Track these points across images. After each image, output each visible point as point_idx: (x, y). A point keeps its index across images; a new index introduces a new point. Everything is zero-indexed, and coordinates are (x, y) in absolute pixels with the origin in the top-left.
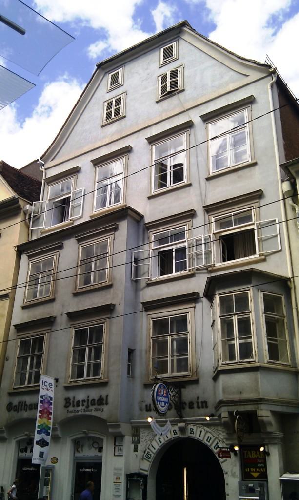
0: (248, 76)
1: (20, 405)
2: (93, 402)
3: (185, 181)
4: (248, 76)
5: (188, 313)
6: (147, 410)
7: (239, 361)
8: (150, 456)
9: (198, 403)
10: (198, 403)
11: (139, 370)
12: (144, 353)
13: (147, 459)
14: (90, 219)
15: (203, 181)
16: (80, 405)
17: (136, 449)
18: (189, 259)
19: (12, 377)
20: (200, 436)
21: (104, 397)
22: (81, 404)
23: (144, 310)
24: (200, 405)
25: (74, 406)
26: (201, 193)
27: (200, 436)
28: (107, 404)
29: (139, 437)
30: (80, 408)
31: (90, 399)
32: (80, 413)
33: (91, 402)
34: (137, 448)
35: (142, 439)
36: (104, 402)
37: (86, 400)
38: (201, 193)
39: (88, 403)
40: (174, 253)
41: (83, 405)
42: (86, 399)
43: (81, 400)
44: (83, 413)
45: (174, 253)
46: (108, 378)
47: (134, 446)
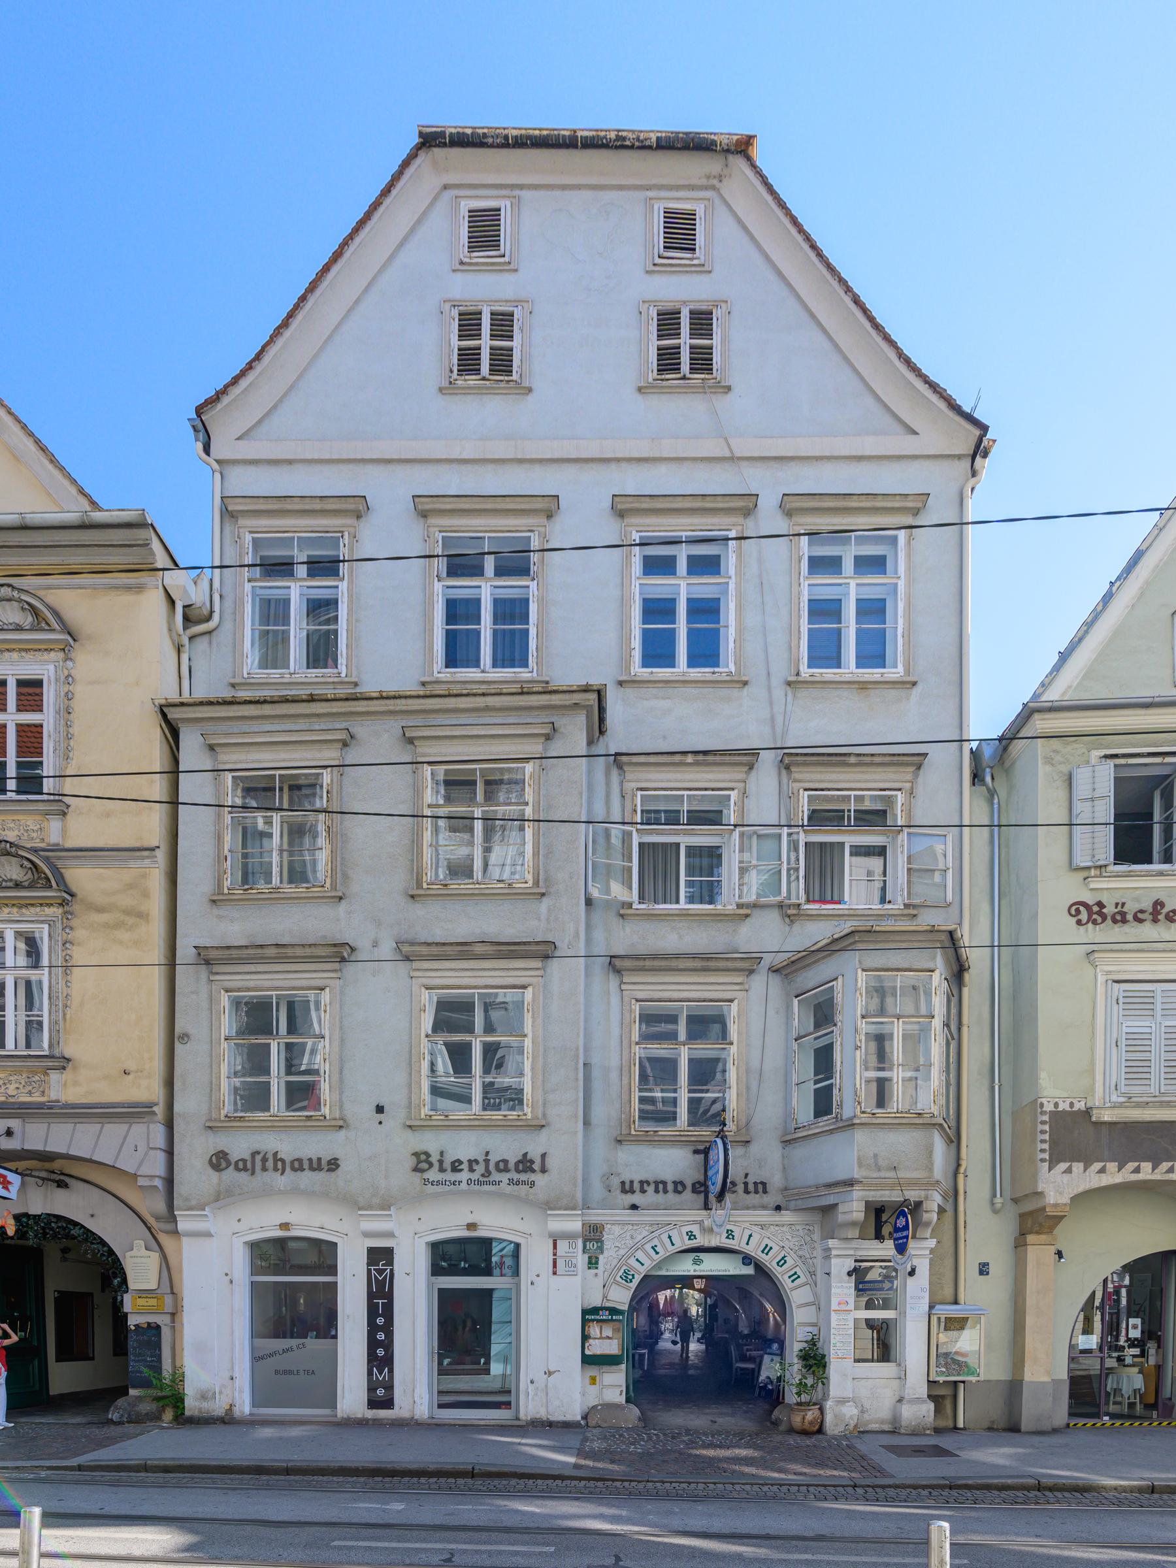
0: (915, 433)
1: (258, 1158)
3: (728, 666)
4: (915, 433)
5: (731, 1001)
6: (624, 1191)
8: (630, 1277)
9: (746, 1184)
10: (746, 1184)
11: (600, 1112)
12: (614, 1075)
17: (593, 1263)
19: (213, 1087)
20: (747, 1244)
21: (535, 1155)
23: (534, 557)
24: (751, 1187)
25: (442, 1170)
26: (773, 719)
28: (544, 1170)
29: (602, 1242)
31: (494, 1159)
34: (597, 1263)
36: (536, 1166)
38: (773, 719)
41: (472, 1170)
42: (481, 1159)
47: (590, 1258)
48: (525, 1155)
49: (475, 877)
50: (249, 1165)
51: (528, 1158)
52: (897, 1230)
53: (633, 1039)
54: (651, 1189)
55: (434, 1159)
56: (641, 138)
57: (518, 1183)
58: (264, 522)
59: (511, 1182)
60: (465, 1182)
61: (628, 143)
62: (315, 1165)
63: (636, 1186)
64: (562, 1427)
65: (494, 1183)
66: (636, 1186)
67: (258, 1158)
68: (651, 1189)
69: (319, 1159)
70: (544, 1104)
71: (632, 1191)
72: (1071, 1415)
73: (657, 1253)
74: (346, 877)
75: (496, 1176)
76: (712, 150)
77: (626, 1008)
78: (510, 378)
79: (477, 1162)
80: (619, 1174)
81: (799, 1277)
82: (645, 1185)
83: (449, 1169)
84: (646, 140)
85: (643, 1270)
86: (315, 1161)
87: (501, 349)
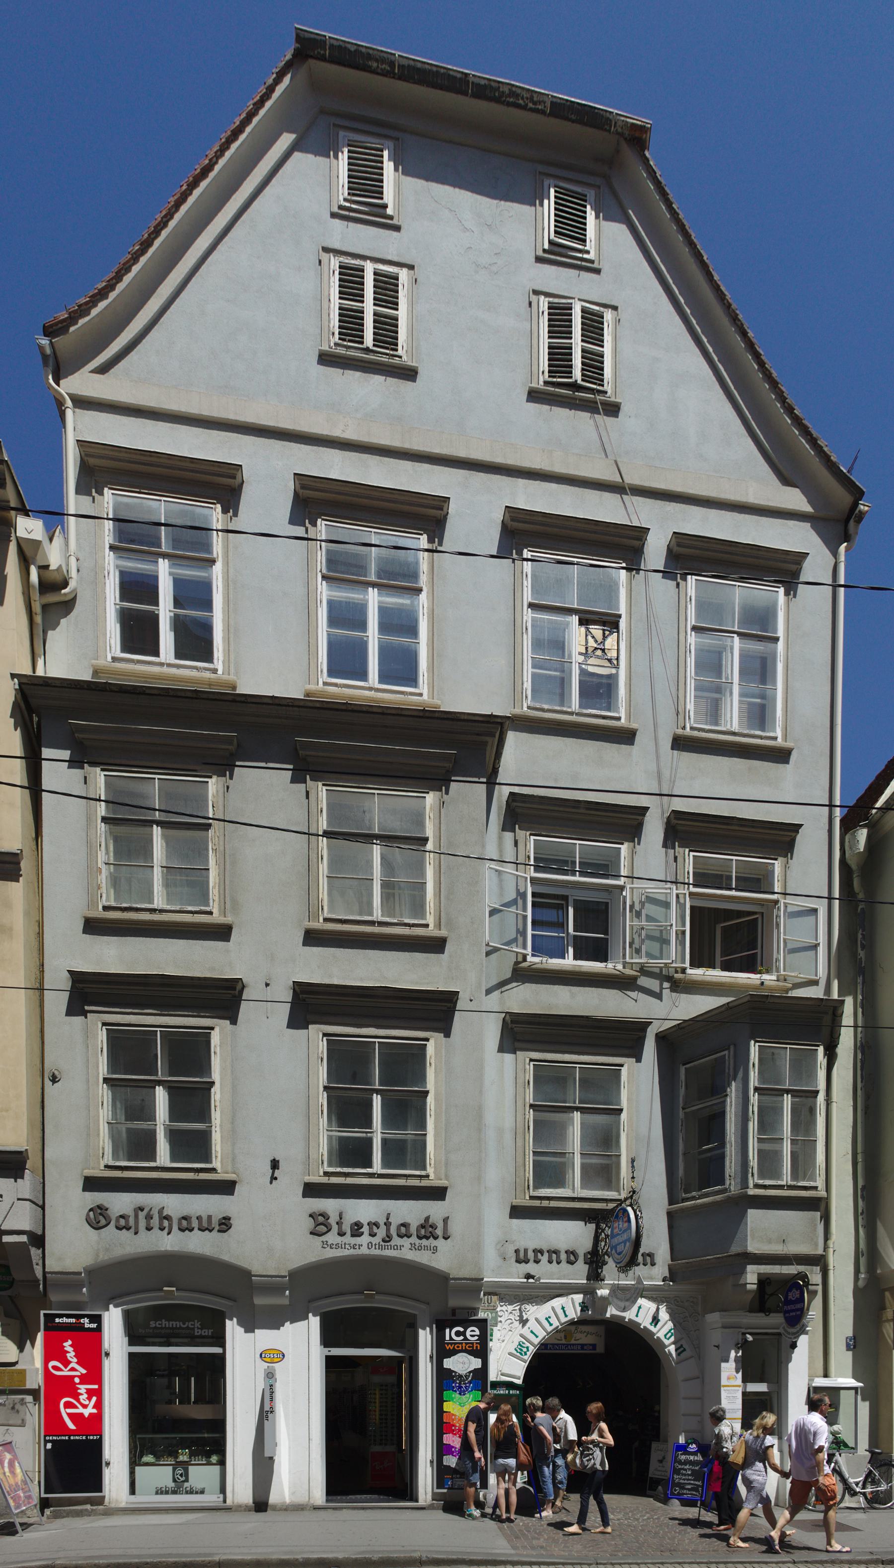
1: (142, 1215)
2: (404, 1230)
6: (518, 1261)
7: (790, 1183)
8: (525, 1350)
12: (508, 1137)
13: (518, 1354)
14: (89, 679)
15: (666, 743)
16: (362, 1234)
18: (524, 933)
19: (90, 1132)
20: (637, 1316)
22: (365, 1229)
25: (341, 1234)
27: (637, 1316)
30: (365, 1239)
31: (395, 1221)
32: (364, 1250)
33: (180, 1223)
35: (501, 1317)
36: (439, 1232)
37: (382, 1223)
39: (388, 1230)
40: (189, 878)
41: (373, 1235)
42: (382, 1221)
43: (365, 1222)
44: (377, 1252)
45: (189, 878)
46: (447, 1177)
48: (427, 1219)
49: (375, 915)
50: (132, 1222)
51: (431, 1221)
52: (787, 1302)
53: (527, 1100)
54: (544, 1258)
55: (333, 1221)
56: (535, 99)
57: (420, 1248)
58: (588, 305)
59: (413, 1247)
60: (365, 1245)
61: (521, 102)
62: (205, 1224)
63: (531, 1255)
64: (245, 1510)
65: (396, 1248)
66: (531, 1255)
67: (142, 1215)
68: (544, 1258)
69: (210, 1217)
70: (446, 1164)
71: (527, 1261)
72: (433, 1500)
73: (551, 1325)
74: (235, 902)
75: (396, 1240)
76: (605, 130)
77: (520, 1066)
78: (395, 353)
79: (377, 1225)
80: (513, 1242)
81: (685, 1350)
82: (539, 1254)
83: (349, 1232)
84: (540, 102)
85: (536, 1341)
86: (205, 1219)
87: (386, 316)
